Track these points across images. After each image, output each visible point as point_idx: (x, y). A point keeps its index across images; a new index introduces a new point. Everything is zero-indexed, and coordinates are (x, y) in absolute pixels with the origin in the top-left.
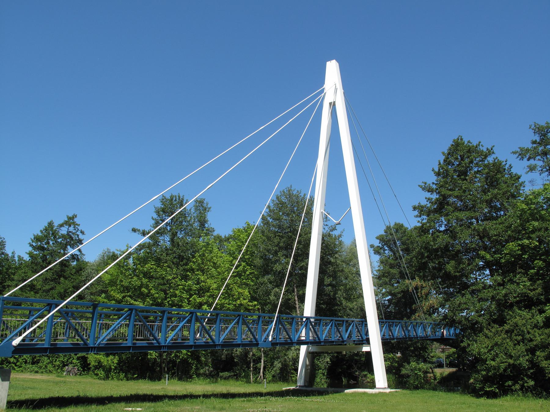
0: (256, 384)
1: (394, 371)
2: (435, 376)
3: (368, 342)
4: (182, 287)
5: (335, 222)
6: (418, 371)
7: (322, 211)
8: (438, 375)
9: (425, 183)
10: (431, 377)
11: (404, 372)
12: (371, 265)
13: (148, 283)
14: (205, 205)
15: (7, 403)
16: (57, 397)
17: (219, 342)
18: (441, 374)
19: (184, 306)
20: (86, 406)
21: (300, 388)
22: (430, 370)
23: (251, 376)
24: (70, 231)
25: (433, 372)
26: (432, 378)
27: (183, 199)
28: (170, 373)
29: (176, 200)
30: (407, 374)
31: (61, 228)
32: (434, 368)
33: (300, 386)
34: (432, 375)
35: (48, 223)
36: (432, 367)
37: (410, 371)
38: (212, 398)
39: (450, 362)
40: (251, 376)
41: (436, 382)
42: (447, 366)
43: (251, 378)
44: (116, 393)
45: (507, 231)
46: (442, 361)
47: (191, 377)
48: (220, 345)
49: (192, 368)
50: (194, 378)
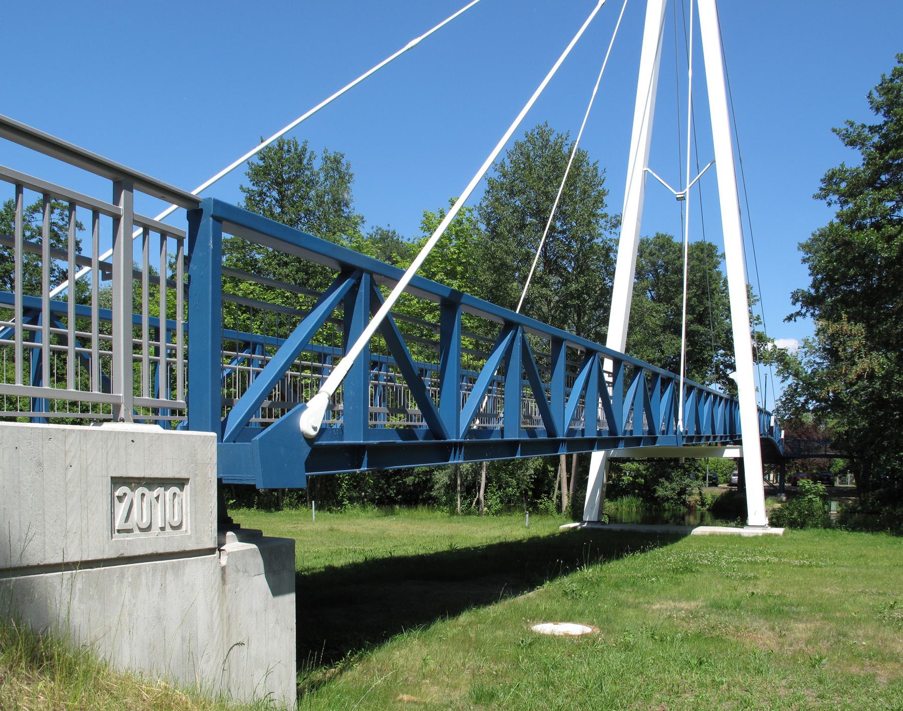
0: (468, 517)
1: (637, 491)
3: (737, 441)
5: (676, 193)
6: (814, 499)
7: (645, 169)
8: (709, 500)
9: (852, 124)
11: (660, 492)
12: (748, 291)
13: (248, 322)
14: (343, 169)
17: (458, 437)
18: (713, 497)
20: (379, 648)
21: (590, 526)
23: (459, 502)
24: (54, 223)
27: (304, 150)
28: (295, 497)
29: (289, 151)
31: (34, 216)
33: (589, 522)
35: (5, 205)
40: (459, 502)
41: (705, 509)
43: (459, 505)
45: (569, 324)
47: (340, 504)
48: (461, 444)
49: (340, 486)
50: (345, 505)
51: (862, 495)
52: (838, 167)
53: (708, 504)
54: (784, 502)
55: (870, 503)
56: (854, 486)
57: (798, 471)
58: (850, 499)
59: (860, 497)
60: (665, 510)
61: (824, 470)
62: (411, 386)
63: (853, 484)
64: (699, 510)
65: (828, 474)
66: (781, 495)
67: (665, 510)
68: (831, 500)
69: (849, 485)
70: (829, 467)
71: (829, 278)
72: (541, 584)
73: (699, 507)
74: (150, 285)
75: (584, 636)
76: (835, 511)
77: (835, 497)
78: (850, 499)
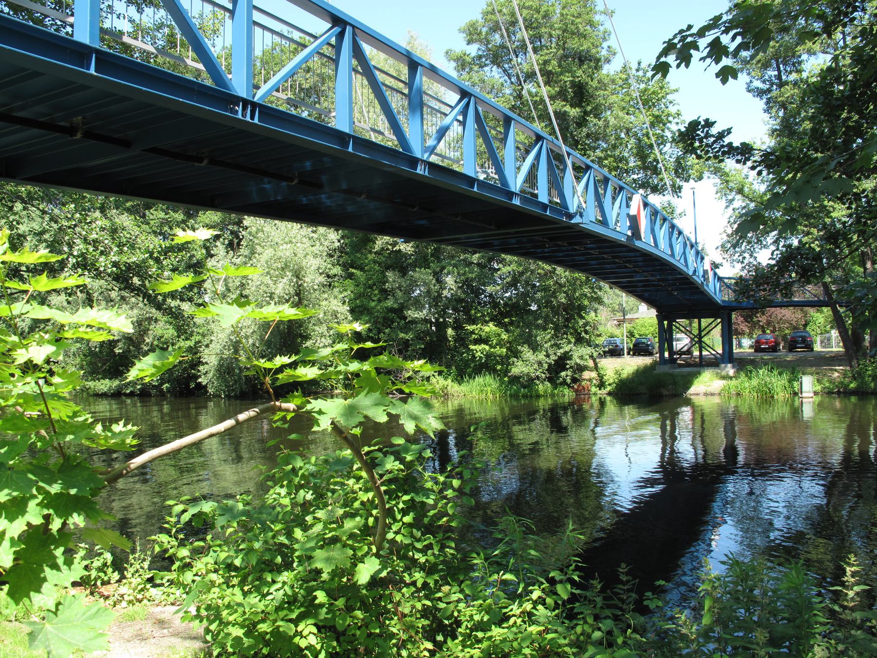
2: (601, 377)
4: (781, 66)
8: (610, 377)
10: (590, 380)
15: (26, 363)
16: (627, 379)
18: (617, 373)
19: (796, 384)
22: (591, 363)
25: (596, 368)
26: (594, 381)
30: (528, 375)
32: (600, 355)
34: (594, 374)
36: (595, 354)
37: (536, 366)
38: (366, 560)
39: (635, 345)
42: (629, 354)
44: (392, 80)
46: (618, 344)
51: (854, 363)
52: (760, 104)
53: (609, 385)
54: (731, 378)
55: (870, 376)
56: (841, 349)
57: (764, 332)
58: (836, 370)
59: (851, 366)
60: (538, 396)
61: (799, 329)
62: (525, 251)
63: (839, 347)
64: (595, 394)
65: (803, 334)
66: (726, 367)
67: (538, 396)
68: (804, 374)
69: (834, 349)
70: (805, 325)
71: (22, 244)
72: (133, 364)
73: (594, 389)
74: (145, 51)
75: (151, 535)
76: (809, 392)
77: (811, 366)
78: (836, 370)
